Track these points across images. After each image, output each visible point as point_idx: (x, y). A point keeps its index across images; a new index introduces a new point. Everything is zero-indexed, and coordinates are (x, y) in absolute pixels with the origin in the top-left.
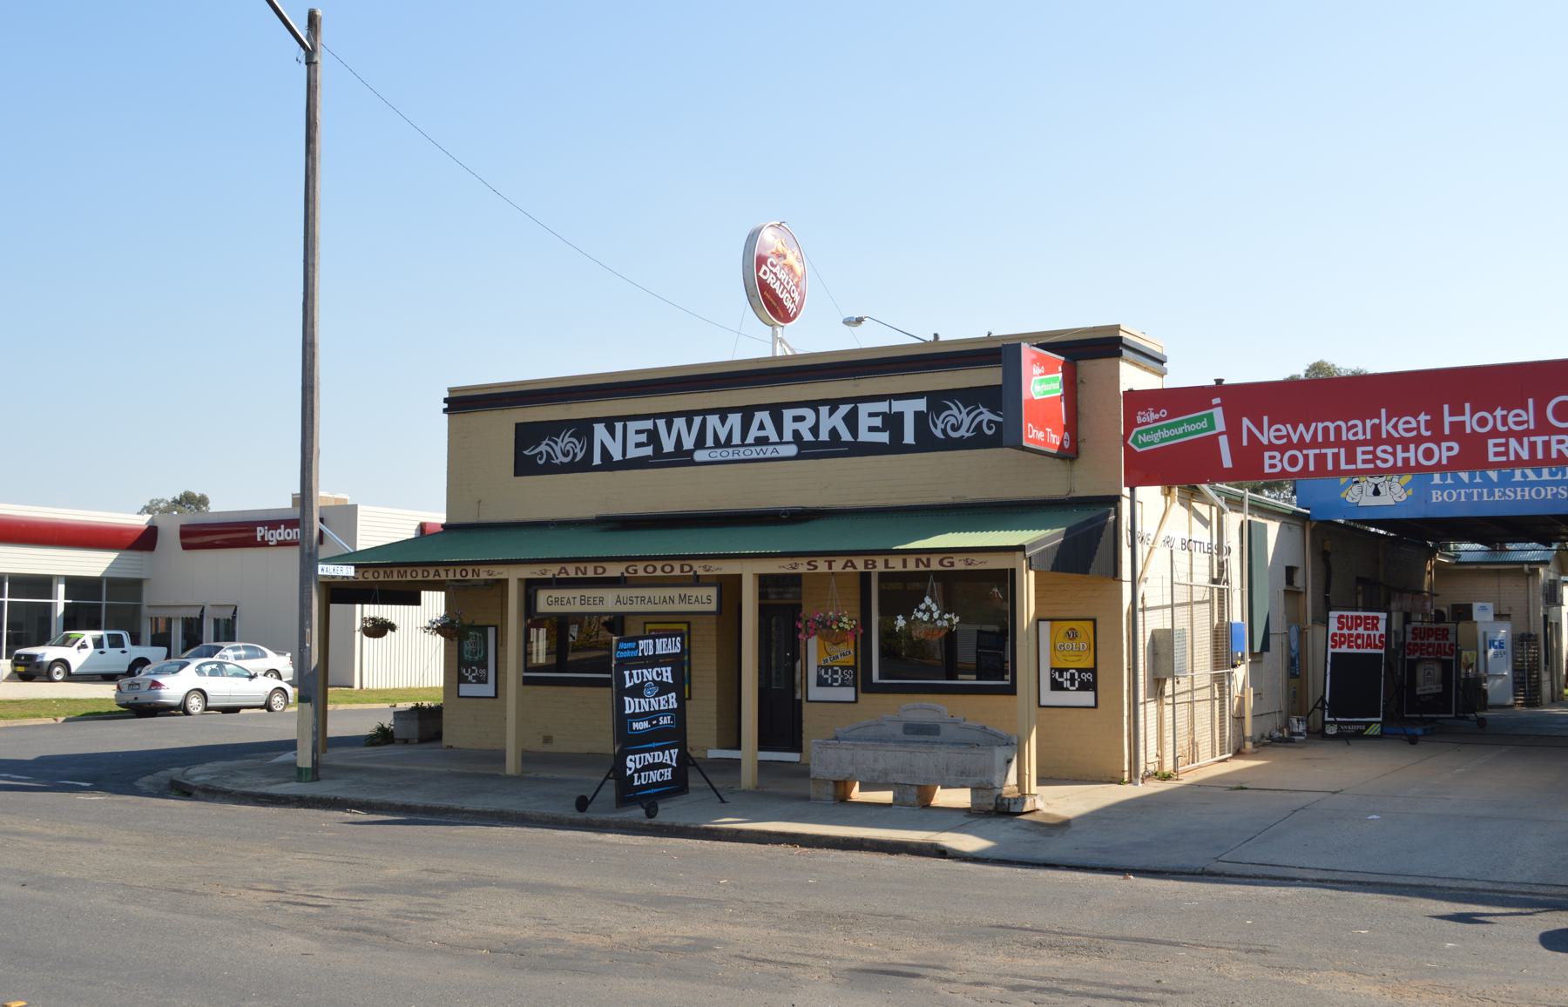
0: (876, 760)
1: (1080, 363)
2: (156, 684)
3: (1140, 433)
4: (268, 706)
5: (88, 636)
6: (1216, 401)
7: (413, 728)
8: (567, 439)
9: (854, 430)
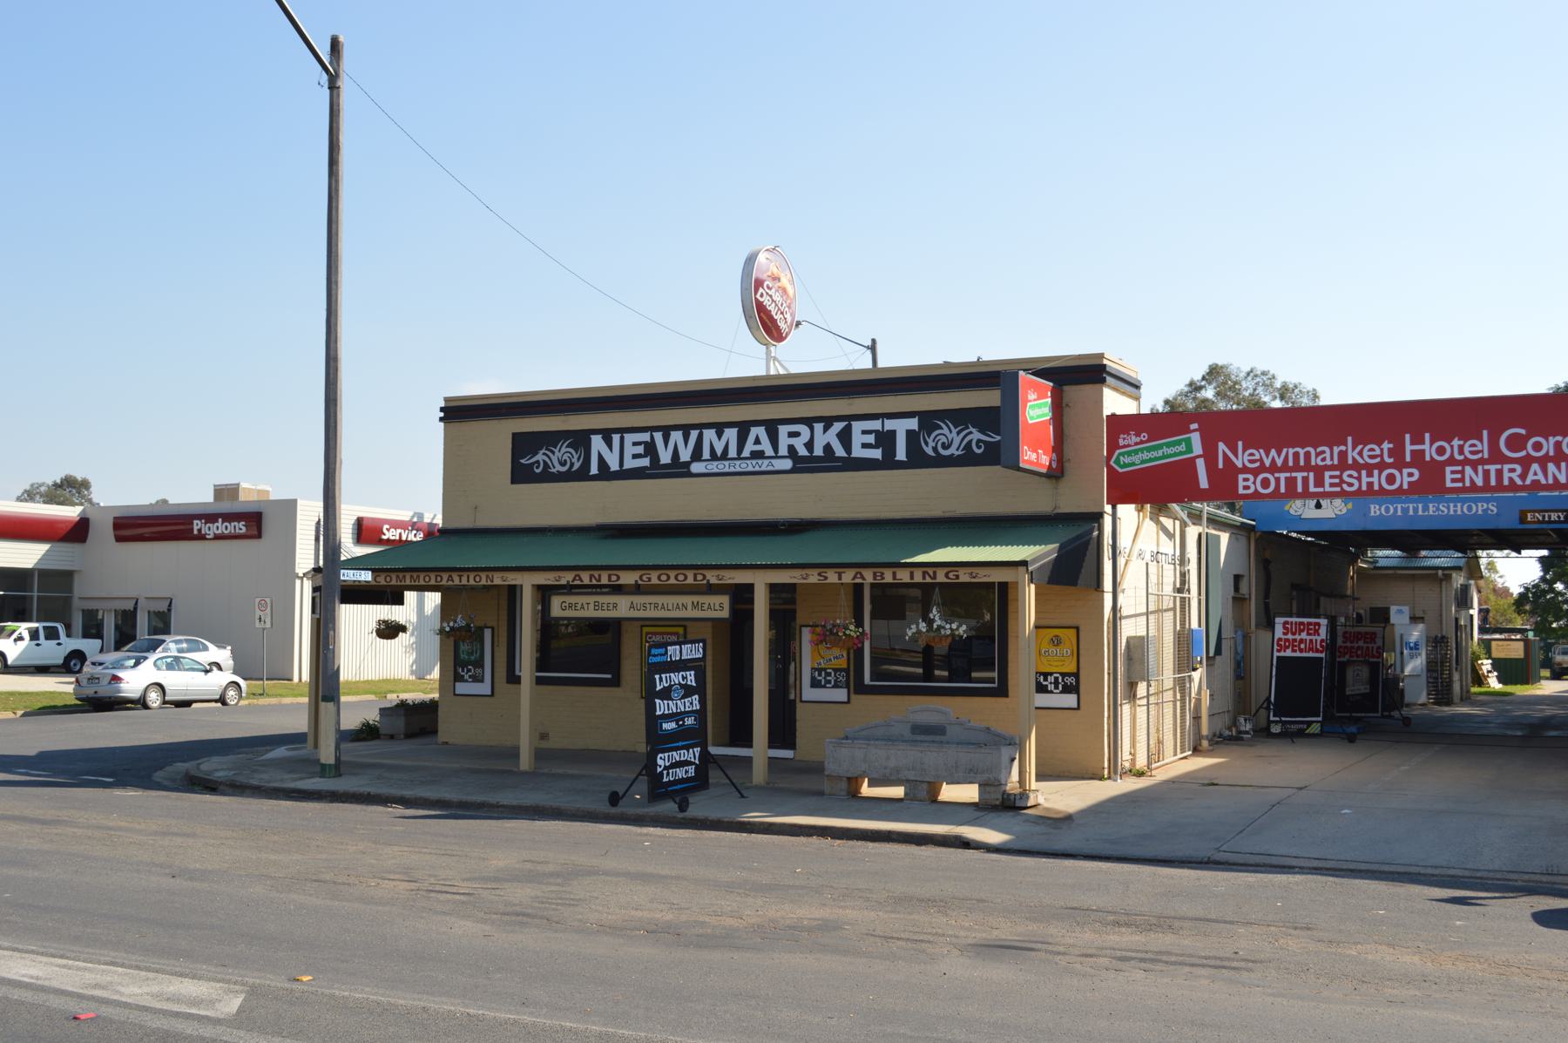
0: (888, 758)
1: (1066, 388)
2: (116, 679)
3: (1122, 454)
4: (222, 700)
5: (23, 628)
6: (1194, 426)
7: (400, 724)
8: (564, 449)
9: (847, 445)
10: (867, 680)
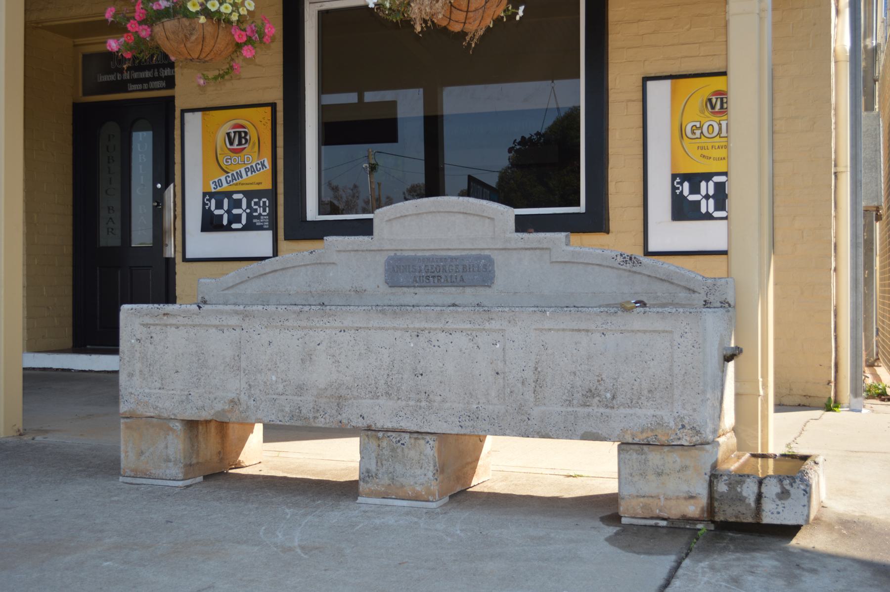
0: (307, 358)
10: (312, 213)
